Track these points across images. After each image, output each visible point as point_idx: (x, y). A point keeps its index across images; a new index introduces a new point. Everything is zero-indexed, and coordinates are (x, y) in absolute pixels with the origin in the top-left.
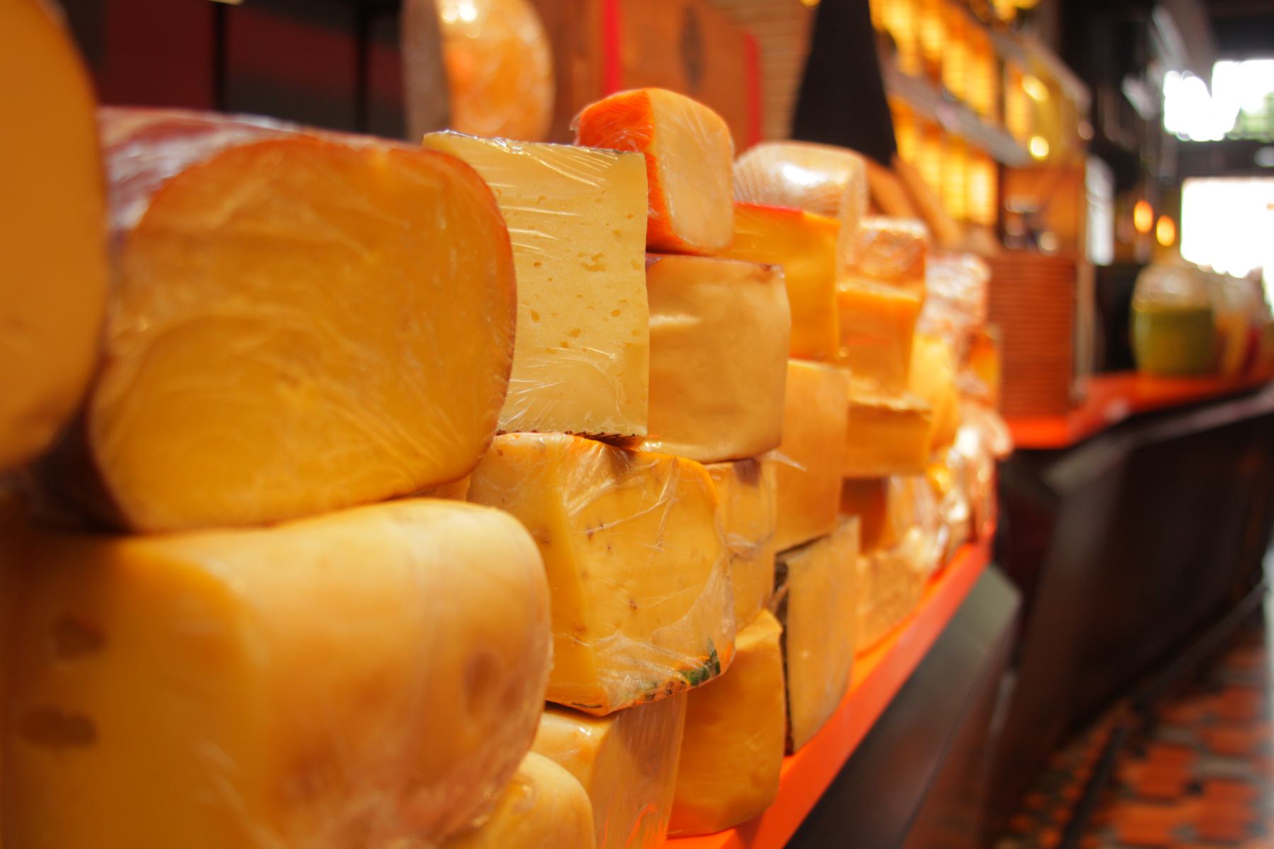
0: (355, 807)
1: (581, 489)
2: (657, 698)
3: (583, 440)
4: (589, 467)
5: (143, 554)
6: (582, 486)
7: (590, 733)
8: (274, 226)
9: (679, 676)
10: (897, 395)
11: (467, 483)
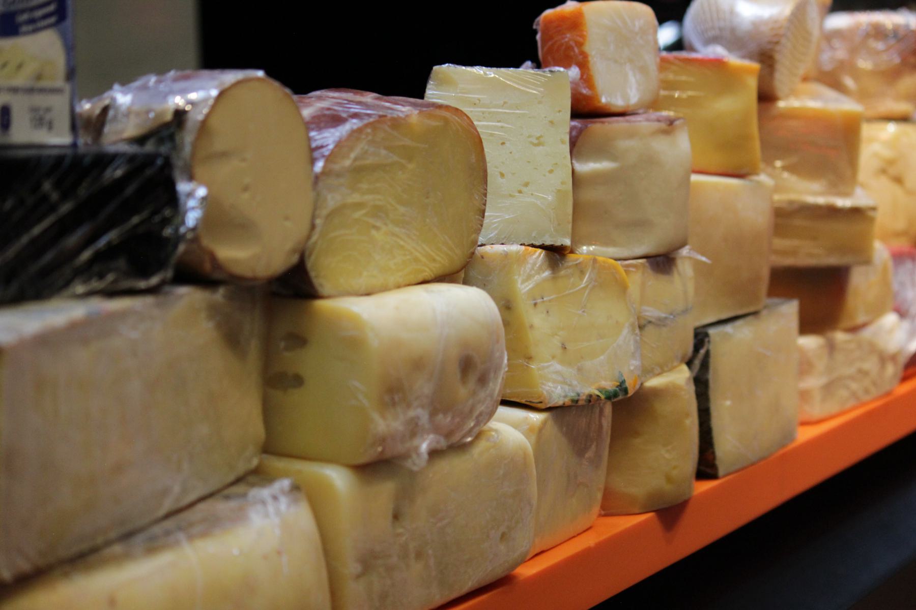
0: (412, 413)
1: (529, 277)
2: (580, 403)
3: (530, 248)
4: (534, 264)
5: (320, 304)
6: (530, 275)
7: (536, 418)
8: (369, 161)
9: (597, 393)
10: (846, 195)
11: (462, 274)
